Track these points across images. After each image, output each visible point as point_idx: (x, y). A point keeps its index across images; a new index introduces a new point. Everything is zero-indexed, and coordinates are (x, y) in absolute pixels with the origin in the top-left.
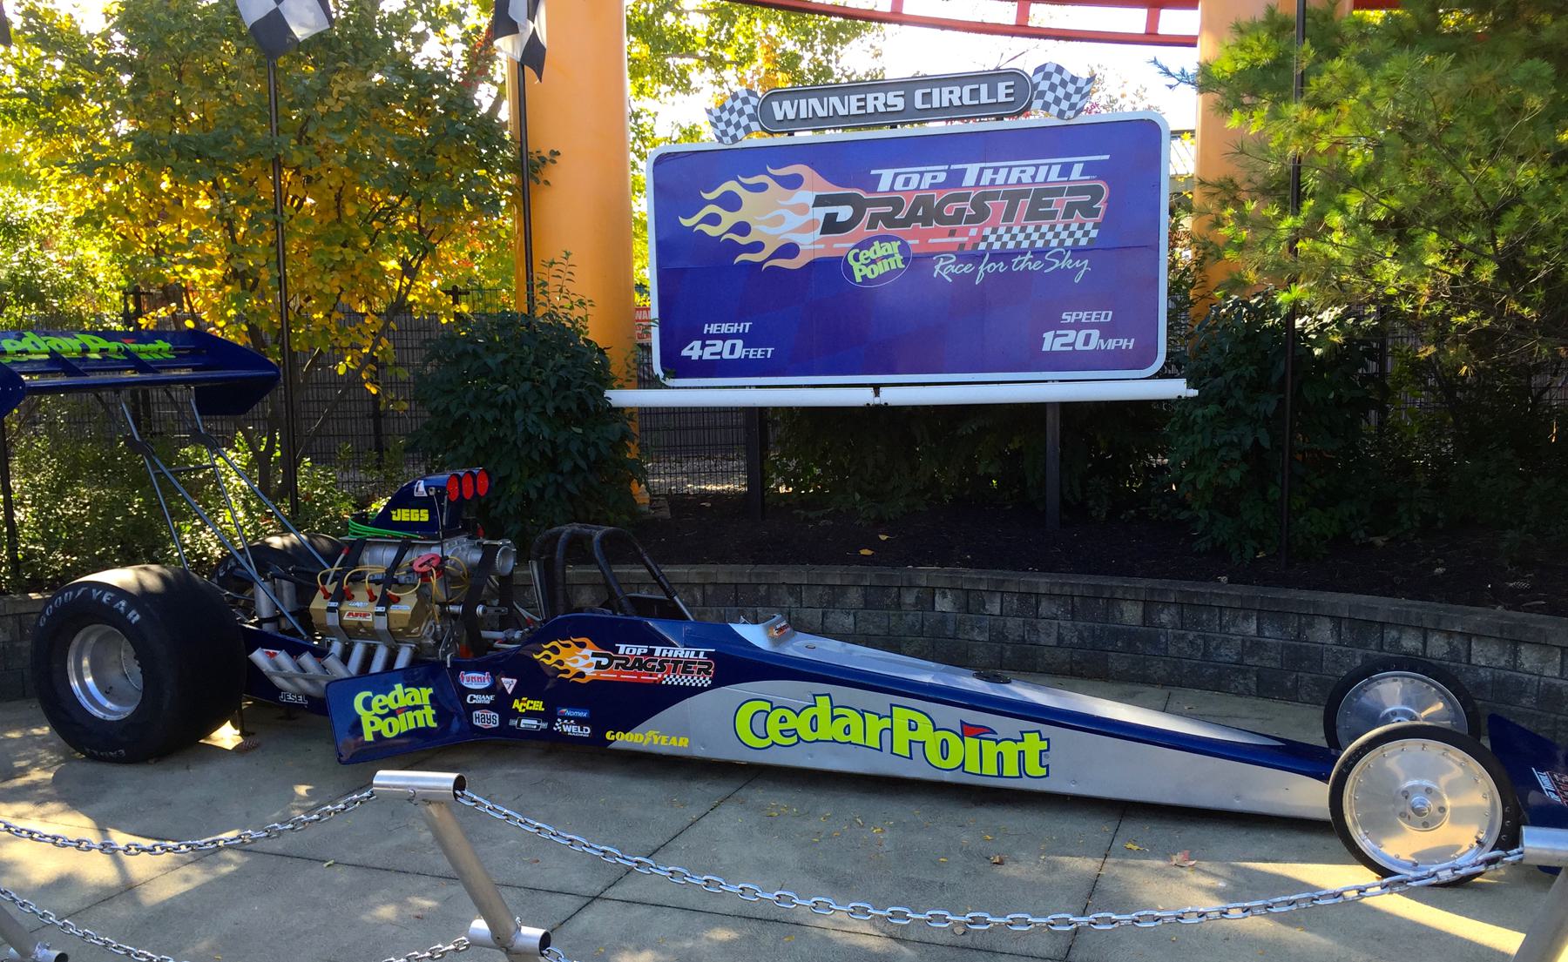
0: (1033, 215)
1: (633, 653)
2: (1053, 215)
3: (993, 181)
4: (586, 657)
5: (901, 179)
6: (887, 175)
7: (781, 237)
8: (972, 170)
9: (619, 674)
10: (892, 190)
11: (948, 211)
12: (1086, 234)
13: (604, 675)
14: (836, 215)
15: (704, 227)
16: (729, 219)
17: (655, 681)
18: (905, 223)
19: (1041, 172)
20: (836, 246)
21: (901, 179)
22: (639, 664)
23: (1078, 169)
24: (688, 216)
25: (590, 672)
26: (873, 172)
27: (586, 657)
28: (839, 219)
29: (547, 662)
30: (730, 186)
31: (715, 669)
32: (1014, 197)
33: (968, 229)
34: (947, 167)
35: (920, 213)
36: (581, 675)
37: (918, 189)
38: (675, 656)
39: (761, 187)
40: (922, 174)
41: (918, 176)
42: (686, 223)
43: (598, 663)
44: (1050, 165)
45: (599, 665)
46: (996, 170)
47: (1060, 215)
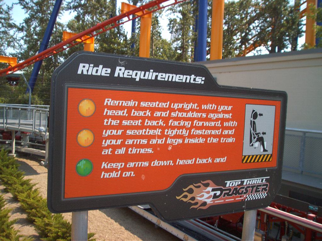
0: (256, 191)
1: (234, 185)
2: (259, 191)
3: (249, 183)
4: (208, 192)
5: (231, 184)
6: (228, 182)
7: (203, 200)
8: (246, 180)
9: (225, 199)
10: (229, 186)
11: (240, 191)
12: (265, 195)
13: (218, 201)
14: (216, 194)
15: (182, 199)
16: (190, 196)
17: (242, 200)
18: (231, 195)
19: (256, 181)
20: (216, 202)
21: (231, 184)
22: (236, 191)
23: (264, 180)
24: (178, 196)
25: (209, 201)
26: (226, 182)
27: (208, 192)
28: (217, 195)
29: (185, 200)
30: (191, 186)
31: (269, 188)
32: (253, 187)
33: (244, 196)
34: (240, 180)
35: (235, 192)
36: (204, 204)
37: (235, 186)
38: (253, 183)
39: (199, 187)
40: (236, 182)
41: (235, 183)
42: (178, 198)
43: (215, 194)
44: (260, 179)
45: (215, 196)
46: (250, 181)
47: (261, 191)
